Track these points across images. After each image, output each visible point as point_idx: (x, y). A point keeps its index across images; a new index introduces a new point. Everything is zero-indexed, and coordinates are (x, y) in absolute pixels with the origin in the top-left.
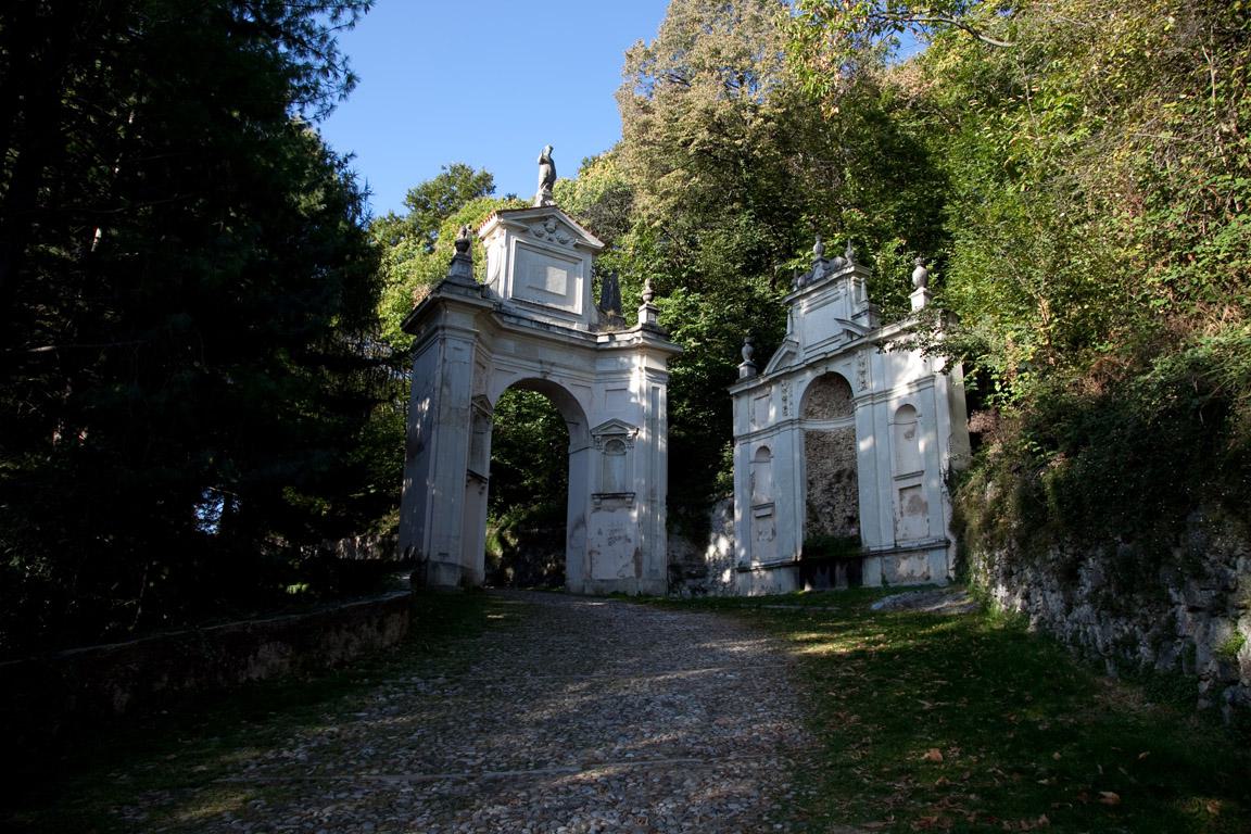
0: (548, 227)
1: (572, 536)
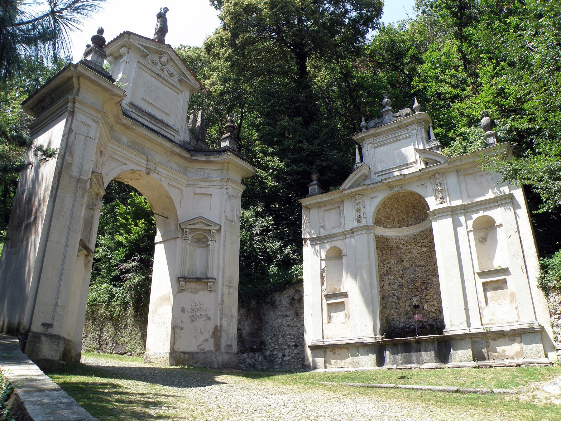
0: (162, 60)
1: (155, 312)
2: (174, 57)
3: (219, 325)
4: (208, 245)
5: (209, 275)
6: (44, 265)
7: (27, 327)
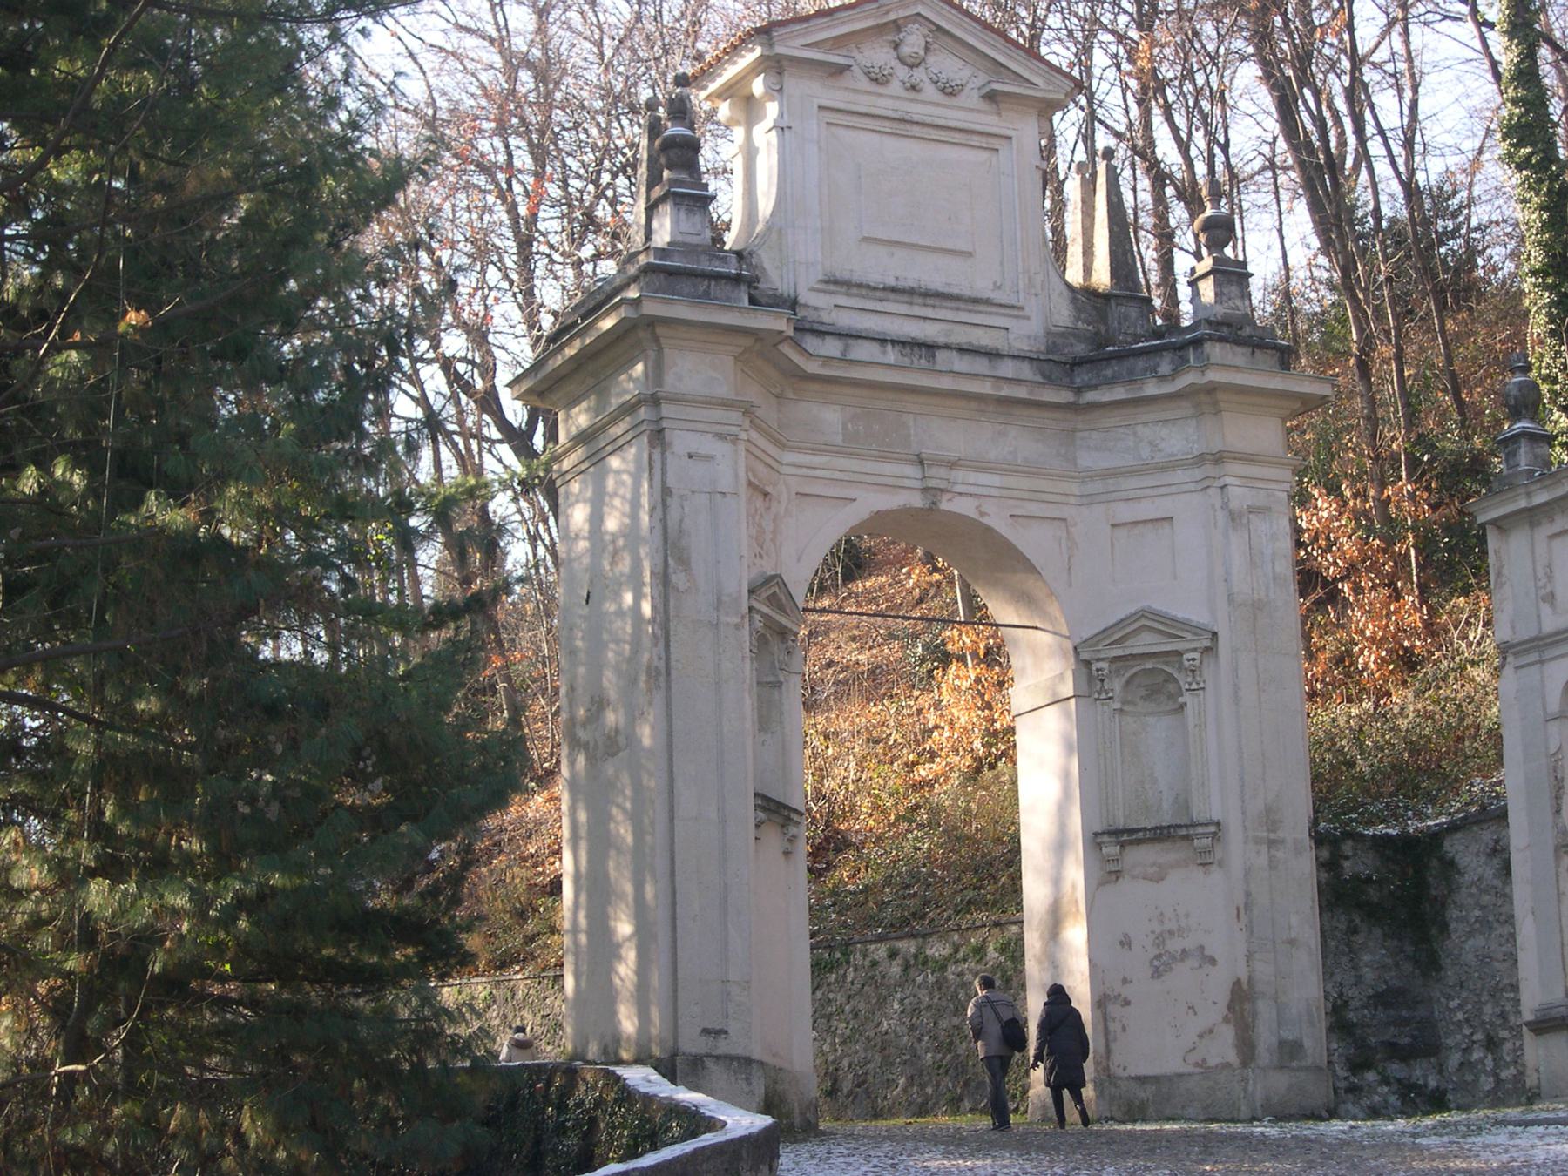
0: (906, 50)
2: (948, 20)
3: (1244, 979)
4: (1183, 706)
5: (1198, 813)
6: (677, 885)
7: (671, 1043)
